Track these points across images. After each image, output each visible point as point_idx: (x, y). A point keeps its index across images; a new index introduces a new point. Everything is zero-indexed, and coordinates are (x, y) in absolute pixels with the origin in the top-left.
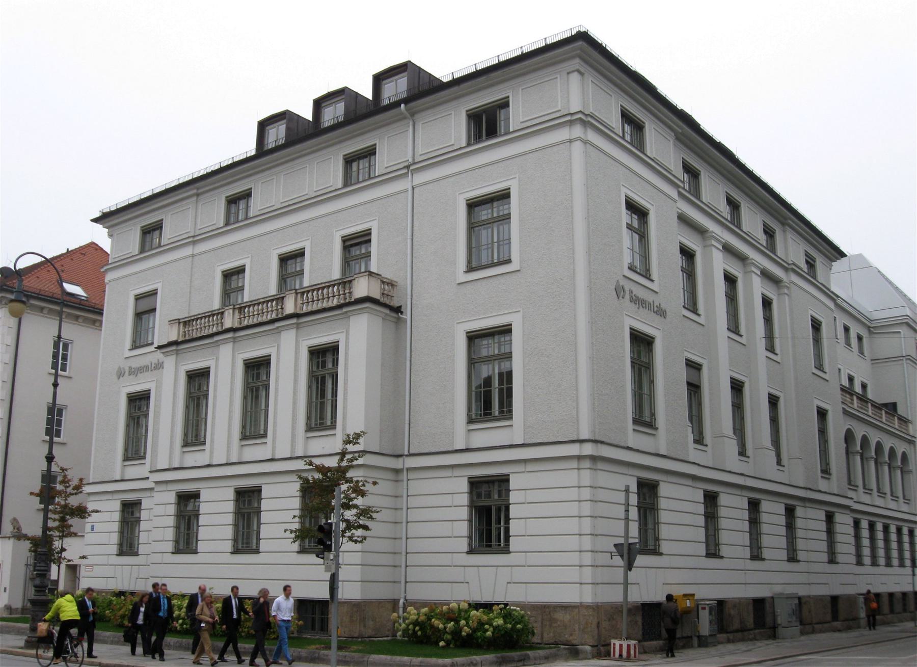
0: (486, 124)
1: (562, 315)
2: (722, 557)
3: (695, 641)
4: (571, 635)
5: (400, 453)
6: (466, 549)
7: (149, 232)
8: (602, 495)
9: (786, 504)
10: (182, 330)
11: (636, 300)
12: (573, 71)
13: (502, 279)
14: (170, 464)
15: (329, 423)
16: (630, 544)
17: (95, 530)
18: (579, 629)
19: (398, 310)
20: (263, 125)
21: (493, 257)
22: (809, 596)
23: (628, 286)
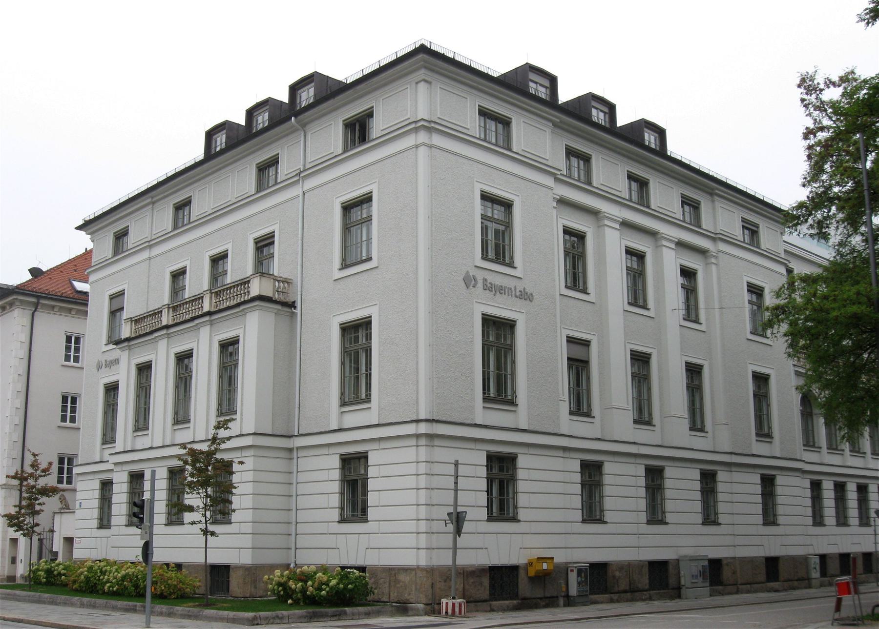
0: (358, 131)
1: (417, 303)
2: (667, 524)
3: (561, 601)
4: (410, 594)
5: (290, 434)
8: (437, 468)
9: (701, 470)
11: (489, 287)
12: (420, 81)
14: (163, 442)
15: (364, 396)
16: (458, 513)
18: (416, 589)
19: (293, 305)
20: (210, 135)
22: (734, 558)
23: (480, 275)
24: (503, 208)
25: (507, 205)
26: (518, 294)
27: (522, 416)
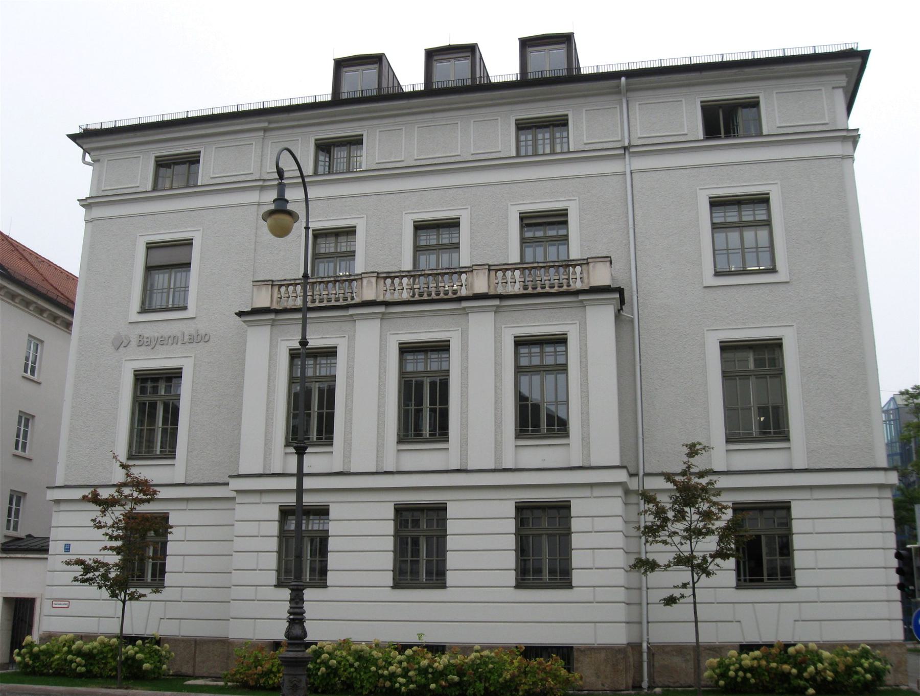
0: (722, 122)
6: (274, 582)
7: (168, 166)
10: (276, 295)
11: (142, 342)
14: (377, 465)
21: (168, 302)
26: (187, 338)
27: (800, 448)
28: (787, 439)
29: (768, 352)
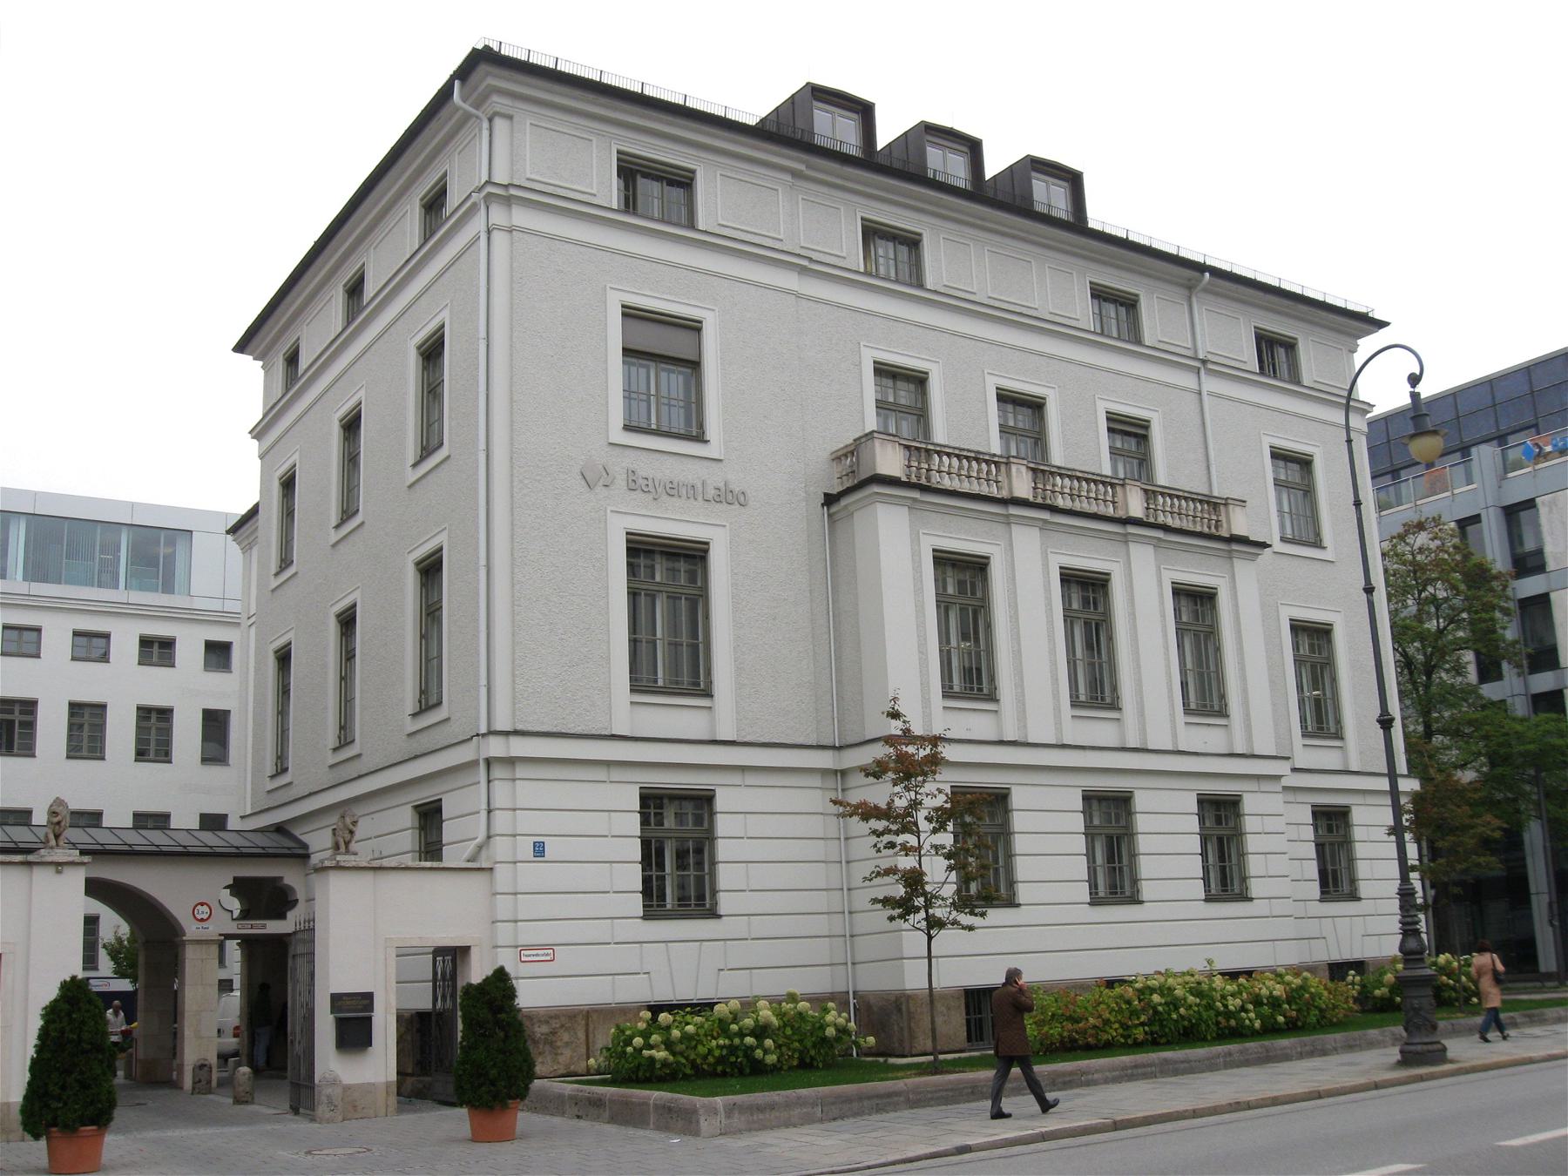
11: (634, 484)
13: (1296, 562)
17: (548, 855)
23: (620, 464)
24: (912, 387)
25: (919, 381)
26: (711, 493)
27: (726, 710)
28: (708, 694)
29: (690, 557)
